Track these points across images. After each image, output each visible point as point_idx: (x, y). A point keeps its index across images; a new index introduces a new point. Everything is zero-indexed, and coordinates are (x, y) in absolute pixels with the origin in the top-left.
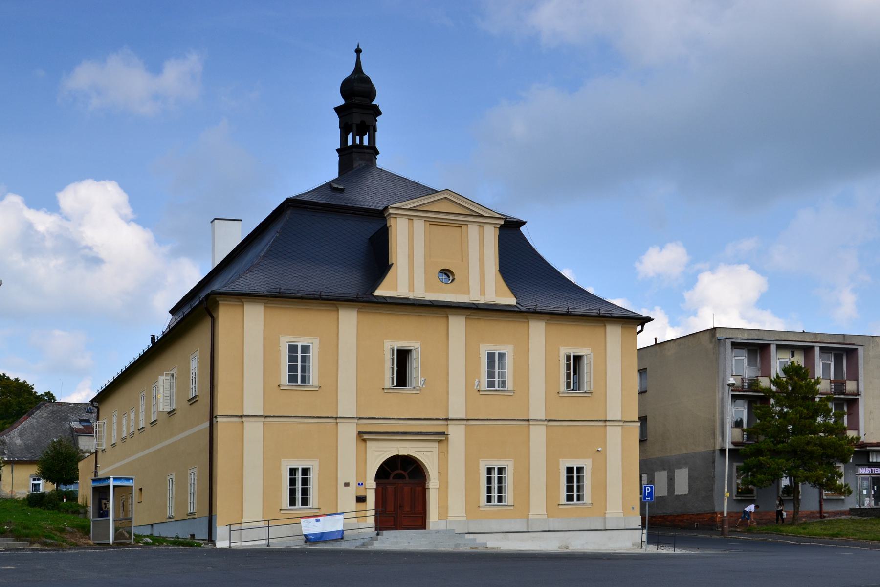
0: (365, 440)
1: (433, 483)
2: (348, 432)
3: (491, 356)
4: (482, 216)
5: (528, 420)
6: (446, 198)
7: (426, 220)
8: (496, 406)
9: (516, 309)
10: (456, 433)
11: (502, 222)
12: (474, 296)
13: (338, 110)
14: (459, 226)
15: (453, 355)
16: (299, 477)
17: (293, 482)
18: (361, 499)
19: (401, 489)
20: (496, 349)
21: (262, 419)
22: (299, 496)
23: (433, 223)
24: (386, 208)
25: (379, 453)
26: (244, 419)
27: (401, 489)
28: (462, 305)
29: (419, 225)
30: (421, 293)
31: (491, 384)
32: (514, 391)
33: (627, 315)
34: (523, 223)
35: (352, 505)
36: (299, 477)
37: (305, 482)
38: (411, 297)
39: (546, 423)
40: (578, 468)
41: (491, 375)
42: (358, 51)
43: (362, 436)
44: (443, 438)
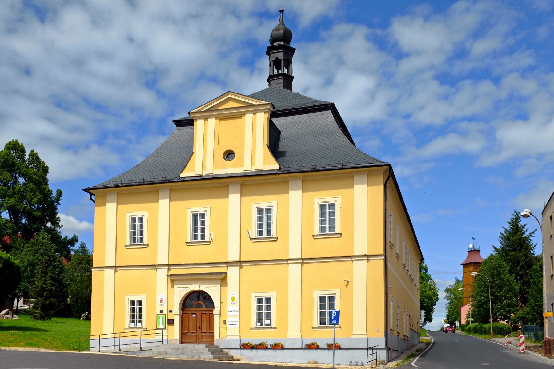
1: (216, 311)
10: (233, 273)
15: (232, 214)
30: (209, 170)
40: (329, 297)
43: (174, 279)
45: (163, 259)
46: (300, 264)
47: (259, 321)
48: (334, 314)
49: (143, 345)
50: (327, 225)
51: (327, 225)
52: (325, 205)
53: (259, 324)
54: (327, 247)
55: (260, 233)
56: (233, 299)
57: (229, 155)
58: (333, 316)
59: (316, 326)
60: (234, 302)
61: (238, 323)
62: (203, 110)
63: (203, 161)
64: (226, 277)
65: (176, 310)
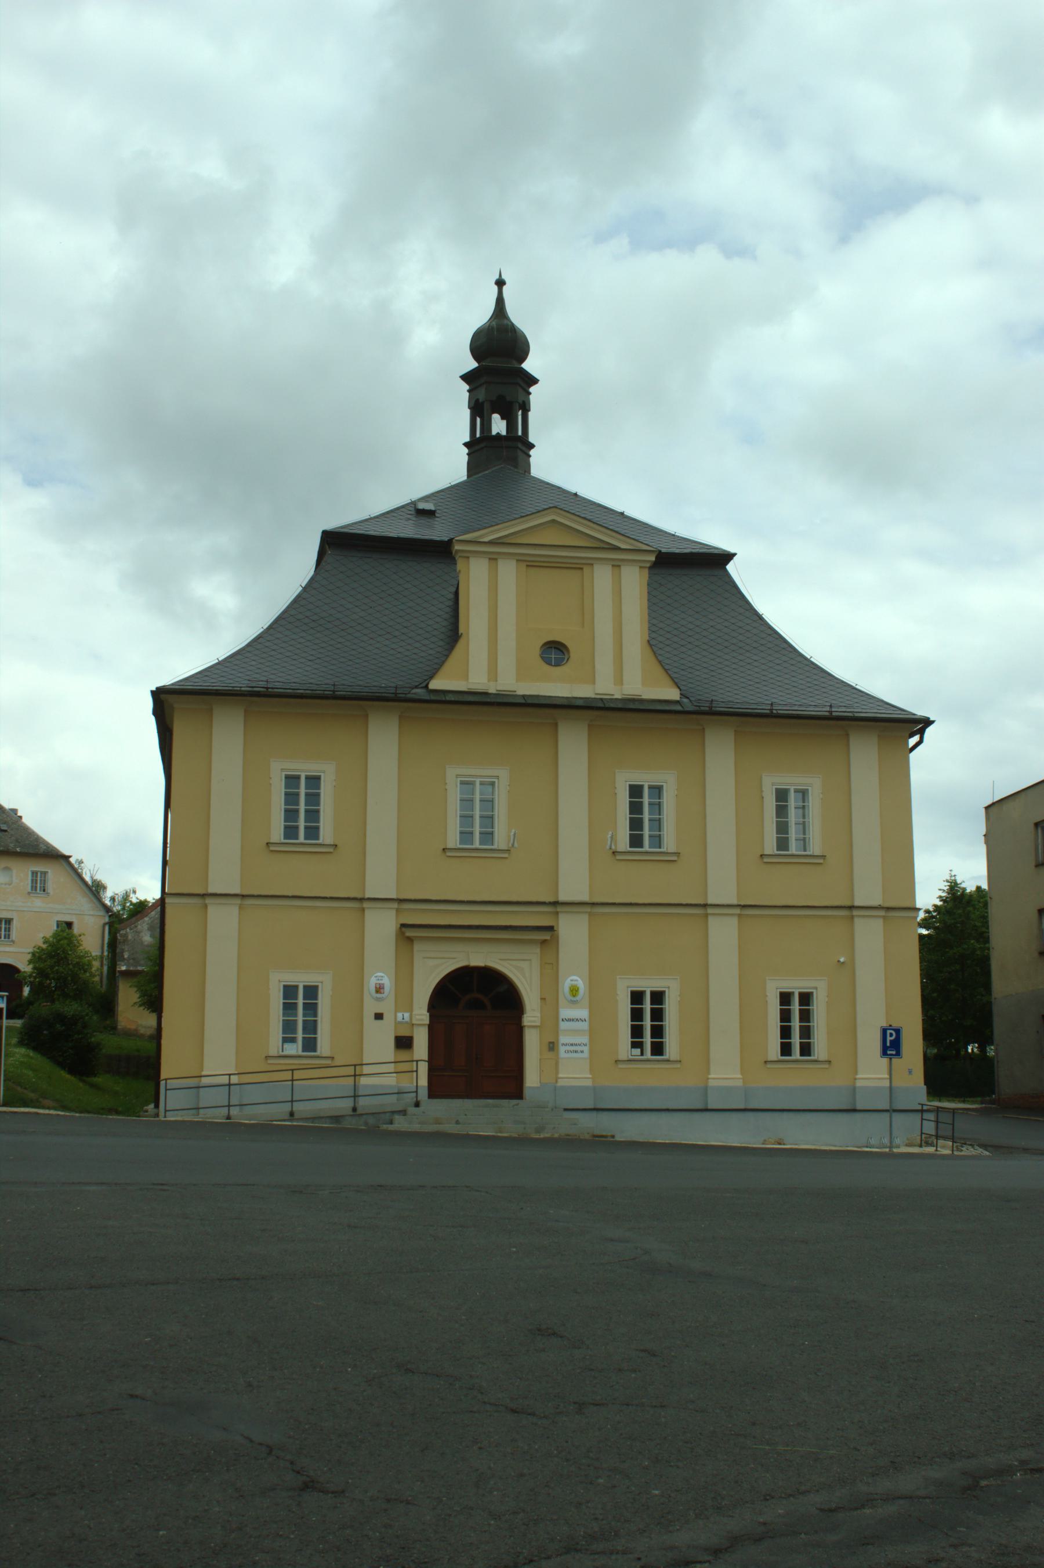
0: (410, 940)
1: (531, 1016)
2: (381, 926)
3: (636, 791)
4: (617, 549)
5: (705, 906)
6: (553, 521)
7: (520, 560)
8: (642, 882)
9: (678, 708)
10: (573, 931)
11: (653, 558)
12: (604, 686)
13: (466, 378)
14: (578, 567)
15: (578, 789)
16: (796, 1007)
17: (637, 1015)
18: (404, 1043)
19: (476, 1026)
20: (645, 778)
21: (238, 901)
22: (796, 1040)
23: (531, 564)
24: (451, 541)
25: (433, 966)
26: (208, 901)
27: (476, 1026)
28: (558, 703)
29: (508, 571)
30: (509, 681)
31: (636, 841)
32: (678, 854)
33: (871, 712)
34: (729, 557)
35: (387, 1050)
36: (796, 1007)
37: (805, 1016)
38: (492, 691)
39: (737, 911)
40: (801, 995)
41: (636, 824)
42: (500, 283)
43: (408, 935)
44: (546, 936)
45: (381, 880)
46: (394, 912)
47: (634, 1045)
48: (891, 1035)
49: (362, 1102)
50: (302, 823)
51: (302, 823)
52: (298, 777)
53: (638, 1051)
54: (301, 874)
55: (291, 832)
56: (379, 989)
57: (555, 651)
58: (889, 1039)
59: (775, 1059)
60: (578, 998)
61: (586, 1049)
62: (486, 539)
63: (490, 656)
64: (555, 940)
65: (422, 1015)
